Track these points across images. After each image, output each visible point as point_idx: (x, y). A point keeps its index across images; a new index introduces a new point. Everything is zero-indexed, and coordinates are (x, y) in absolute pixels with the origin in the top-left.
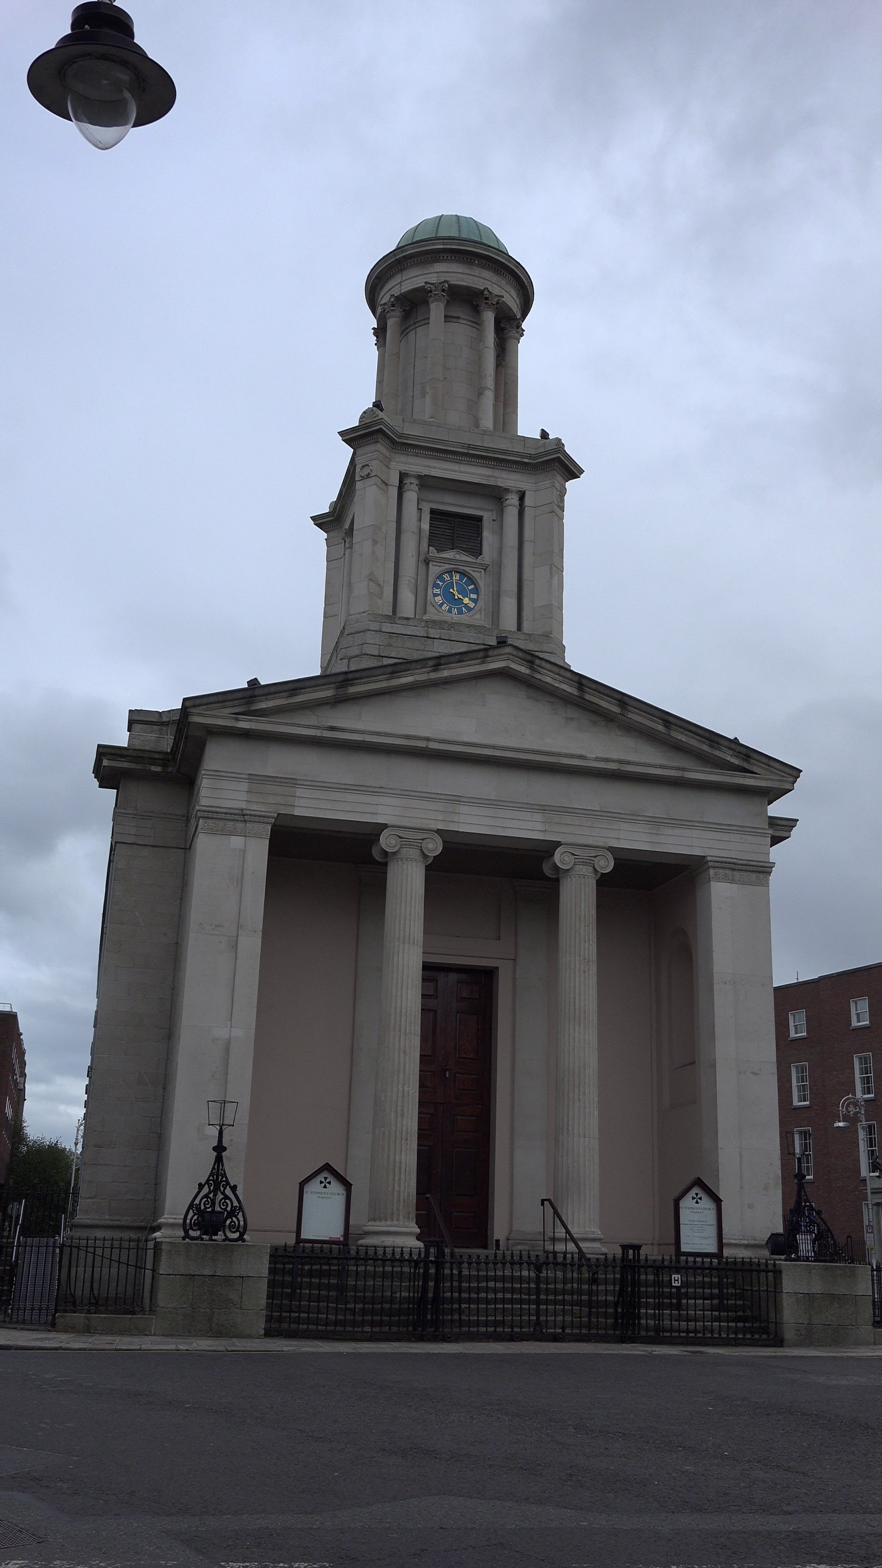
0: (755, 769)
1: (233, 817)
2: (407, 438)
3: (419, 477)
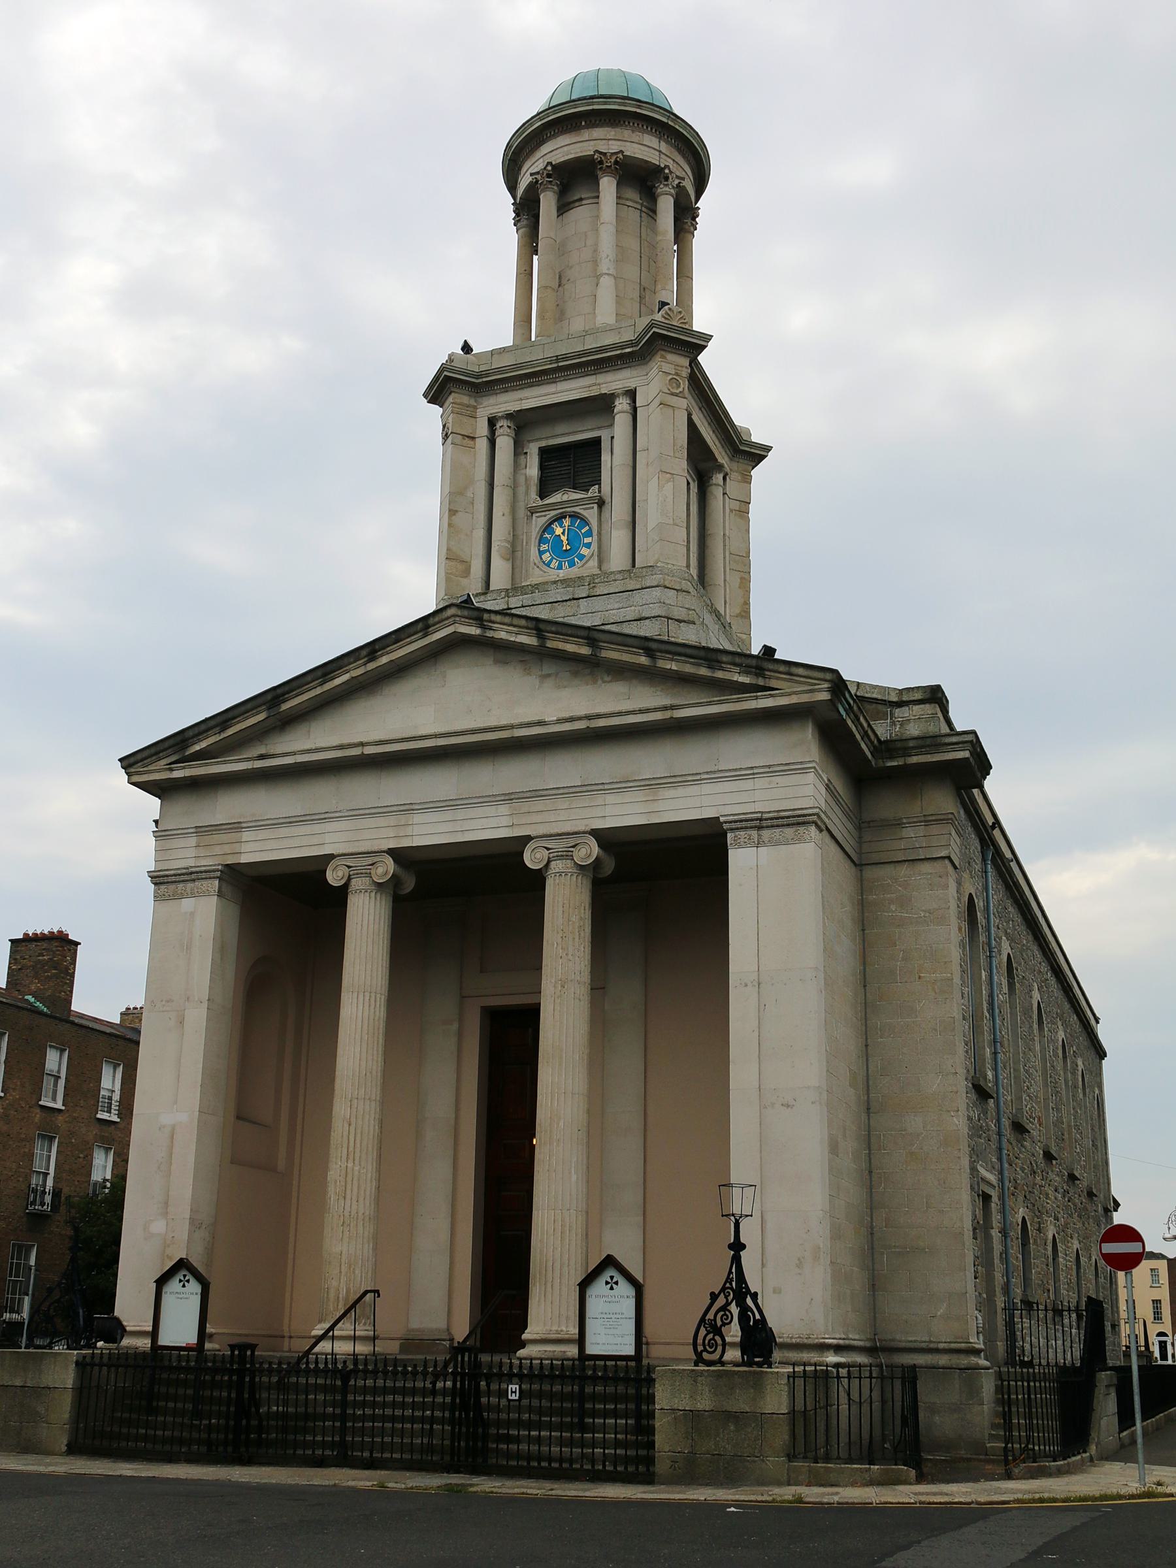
0: (773, 683)
1: (182, 878)
2: (487, 375)
3: (509, 416)
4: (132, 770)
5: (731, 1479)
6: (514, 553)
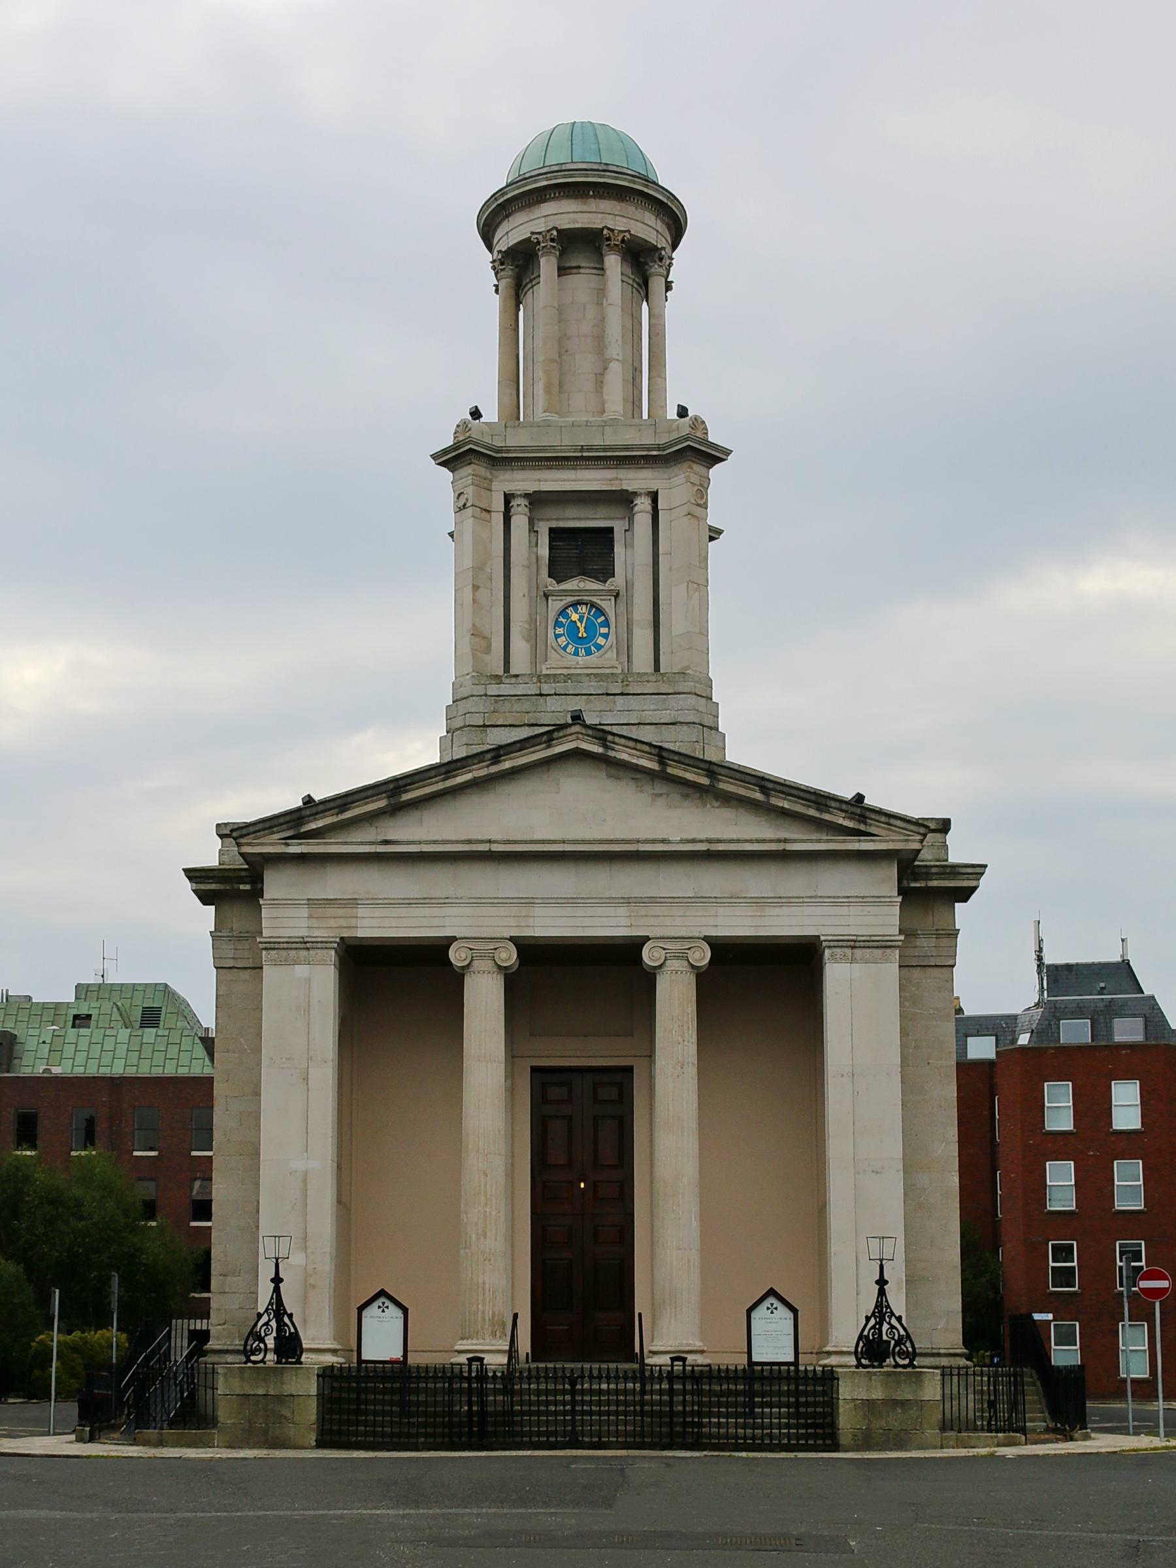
0: (873, 830)
1: (294, 946)
2: (508, 451)
3: (527, 496)
4: (242, 841)
5: (900, 1447)
6: (534, 638)
